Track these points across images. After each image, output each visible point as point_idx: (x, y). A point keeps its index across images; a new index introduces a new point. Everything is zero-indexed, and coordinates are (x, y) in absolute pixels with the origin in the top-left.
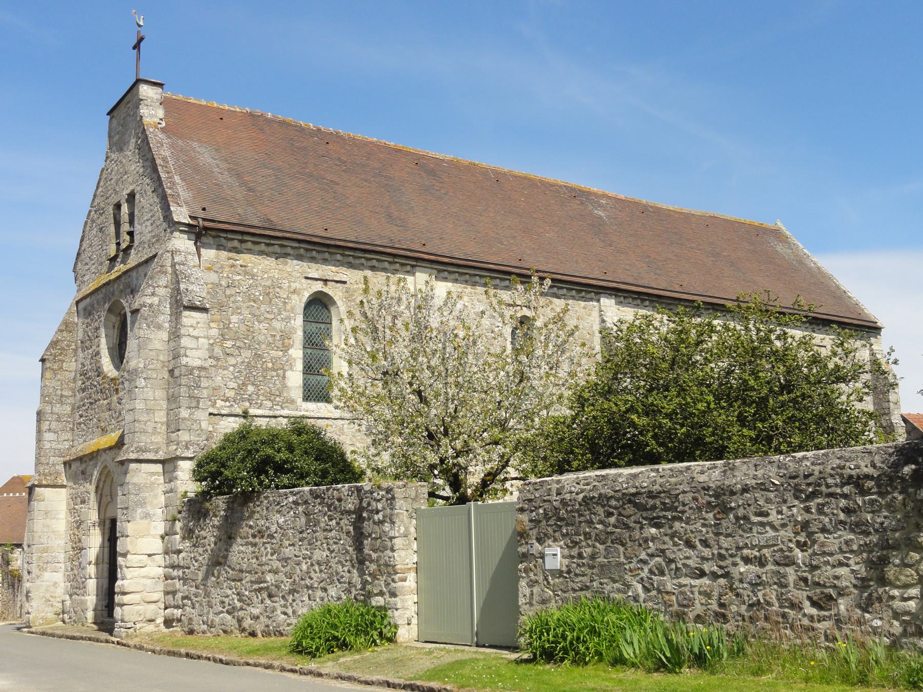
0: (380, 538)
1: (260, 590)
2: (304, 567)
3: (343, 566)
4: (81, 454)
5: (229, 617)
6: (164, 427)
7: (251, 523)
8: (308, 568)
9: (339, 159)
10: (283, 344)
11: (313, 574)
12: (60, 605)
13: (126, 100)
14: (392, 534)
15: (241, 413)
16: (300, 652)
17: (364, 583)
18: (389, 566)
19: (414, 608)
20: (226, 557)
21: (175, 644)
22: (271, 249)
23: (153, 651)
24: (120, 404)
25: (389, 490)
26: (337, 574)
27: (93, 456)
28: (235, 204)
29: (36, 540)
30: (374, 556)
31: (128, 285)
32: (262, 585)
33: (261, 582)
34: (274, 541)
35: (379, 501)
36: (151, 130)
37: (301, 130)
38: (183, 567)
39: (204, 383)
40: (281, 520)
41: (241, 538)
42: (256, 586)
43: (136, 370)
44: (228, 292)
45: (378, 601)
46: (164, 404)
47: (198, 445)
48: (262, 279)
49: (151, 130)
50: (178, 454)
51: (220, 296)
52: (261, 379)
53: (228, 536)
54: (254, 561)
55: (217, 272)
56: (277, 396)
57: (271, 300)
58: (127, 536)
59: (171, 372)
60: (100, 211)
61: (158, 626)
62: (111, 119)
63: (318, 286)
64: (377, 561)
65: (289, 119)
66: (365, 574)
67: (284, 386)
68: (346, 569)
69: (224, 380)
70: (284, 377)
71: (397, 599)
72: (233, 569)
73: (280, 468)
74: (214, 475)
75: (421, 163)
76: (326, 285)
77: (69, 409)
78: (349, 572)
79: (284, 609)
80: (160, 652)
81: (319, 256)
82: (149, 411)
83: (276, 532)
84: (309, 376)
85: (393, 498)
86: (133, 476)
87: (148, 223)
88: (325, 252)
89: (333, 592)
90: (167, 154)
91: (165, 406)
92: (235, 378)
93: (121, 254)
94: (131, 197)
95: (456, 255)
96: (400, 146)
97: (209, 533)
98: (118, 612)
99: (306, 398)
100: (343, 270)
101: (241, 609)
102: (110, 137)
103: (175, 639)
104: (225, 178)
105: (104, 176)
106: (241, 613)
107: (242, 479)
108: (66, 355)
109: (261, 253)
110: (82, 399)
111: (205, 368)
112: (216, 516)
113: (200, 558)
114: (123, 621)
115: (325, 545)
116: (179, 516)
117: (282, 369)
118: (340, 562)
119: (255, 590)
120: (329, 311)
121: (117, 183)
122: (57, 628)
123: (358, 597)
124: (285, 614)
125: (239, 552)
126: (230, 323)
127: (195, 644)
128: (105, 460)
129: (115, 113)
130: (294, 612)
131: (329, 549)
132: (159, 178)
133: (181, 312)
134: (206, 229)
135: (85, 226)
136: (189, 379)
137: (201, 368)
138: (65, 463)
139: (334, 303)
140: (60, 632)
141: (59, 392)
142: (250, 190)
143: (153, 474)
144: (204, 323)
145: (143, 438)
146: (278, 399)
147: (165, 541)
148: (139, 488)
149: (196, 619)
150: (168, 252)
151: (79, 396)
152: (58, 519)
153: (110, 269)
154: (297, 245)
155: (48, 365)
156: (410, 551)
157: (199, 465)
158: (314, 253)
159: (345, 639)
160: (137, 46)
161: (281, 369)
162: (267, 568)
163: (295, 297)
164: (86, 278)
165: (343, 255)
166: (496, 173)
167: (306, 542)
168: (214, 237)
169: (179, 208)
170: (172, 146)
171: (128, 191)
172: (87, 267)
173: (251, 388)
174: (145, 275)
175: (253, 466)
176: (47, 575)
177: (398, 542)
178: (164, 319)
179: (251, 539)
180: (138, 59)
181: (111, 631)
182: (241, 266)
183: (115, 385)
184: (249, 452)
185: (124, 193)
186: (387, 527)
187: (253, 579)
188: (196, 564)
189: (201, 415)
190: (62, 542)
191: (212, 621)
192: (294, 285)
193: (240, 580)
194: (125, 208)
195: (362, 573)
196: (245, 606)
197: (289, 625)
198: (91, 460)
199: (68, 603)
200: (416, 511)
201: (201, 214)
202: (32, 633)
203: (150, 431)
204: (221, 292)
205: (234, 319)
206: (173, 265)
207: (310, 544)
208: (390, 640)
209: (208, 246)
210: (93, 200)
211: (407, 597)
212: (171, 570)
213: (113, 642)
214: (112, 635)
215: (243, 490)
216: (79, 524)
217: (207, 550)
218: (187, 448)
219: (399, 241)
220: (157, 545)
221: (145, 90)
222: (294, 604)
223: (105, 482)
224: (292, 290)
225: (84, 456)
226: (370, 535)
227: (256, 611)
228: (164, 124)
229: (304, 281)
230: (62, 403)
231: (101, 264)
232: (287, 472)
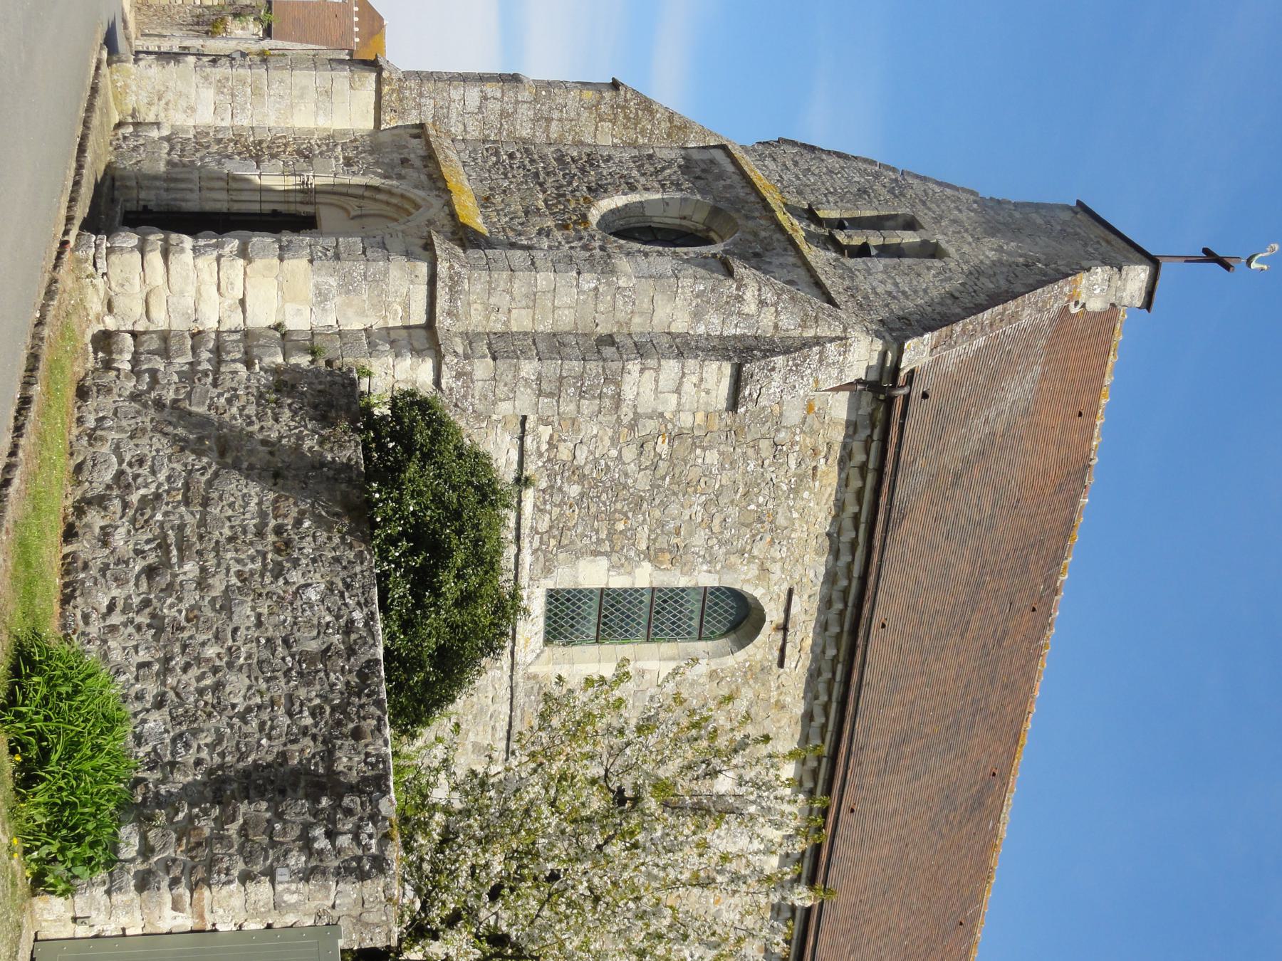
0: (273, 844)
1: (163, 546)
2: (211, 652)
3: (212, 747)
4: (441, 158)
5: (108, 477)
6: (499, 328)
7: (307, 524)
8: (208, 660)
9: (1005, 633)
10: (662, 550)
11: (194, 671)
12: (151, 118)
13: (1112, 237)
14: (282, 874)
15: (526, 473)
16: (15, 670)
17: (168, 802)
18: (209, 871)
19: (112, 929)
20: (236, 466)
21: (55, 365)
22: (848, 523)
23: (40, 323)
24: (540, 233)
25: (380, 864)
26: (195, 733)
27: (438, 183)
28: (932, 453)
29: (276, 74)
30: (232, 829)
31: (768, 247)
32: (175, 552)
33: (180, 550)
34: (268, 580)
35: (356, 838)
36: (1067, 289)
37: (1057, 559)
38: (217, 372)
39: (588, 406)
40: (312, 595)
41: (276, 501)
42: (172, 537)
43: (612, 272)
44: (765, 444)
45: (130, 841)
46: (545, 326)
47: (465, 397)
48: (790, 509)
49: (1067, 289)
50: (448, 359)
51: (755, 431)
52: (593, 510)
53: (281, 470)
54: (227, 532)
55: (804, 422)
56: (559, 540)
57: (748, 526)
58: (281, 259)
59: (609, 340)
60: (897, 189)
61: (99, 319)
62: (1068, 208)
63: (774, 614)
64: (221, 838)
65: (1077, 536)
66: (191, 806)
67: (579, 555)
68: (204, 754)
69: (593, 438)
70: (596, 553)
71: (132, 894)
72: (210, 483)
73: (423, 581)
74: (405, 438)
75: (997, 777)
76: (777, 629)
77: (525, 133)
78: (198, 762)
79: (120, 604)
80: (37, 338)
81: (832, 615)
82: (533, 299)
83: (287, 583)
84: (597, 599)
85: (363, 876)
86: (402, 268)
87: (890, 287)
88: (842, 627)
89: (155, 722)
90: (1025, 320)
91: (541, 328)
92: (596, 462)
93: (825, 232)
94: (932, 251)
95: (834, 872)
96: (1024, 740)
97: (283, 426)
98: (128, 239)
99: (552, 595)
100: (806, 660)
101: (126, 505)
102: (1037, 207)
103: (68, 363)
104: (978, 428)
105: (964, 196)
106: (116, 505)
107: (399, 501)
108: (626, 127)
109: (840, 505)
110: (543, 158)
111: (618, 407)
112: (321, 443)
113: (234, 410)
114: (110, 251)
115: (258, 700)
116: (322, 363)
117: (612, 548)
118: (220, 738)
119: (165, 537)
120: (723, 635)
121: (954, 221)
122: (107, 114)
123: (140, 789)
124: (111, 608)
125: (244, 498)
126: (704, 449)
127: (56, 396)
128: (431, 206)
129: (1081, 216)
130: (113, 629)
131: (249, 710)
132: (981, 308)
133: (730, 359)
134: (890, 401)
135: (865, 161)
136: (598, 375)
137: (618, 399)
138: (422, 126)
139: (741, 645)
140: (96, 120)
141: (556, 115)
142: (957, 477)
143: (407, 307)
144: (707, 404)
145: (478, 287)
146: (553, 542)
147: (272, 332)
148: (377, 282)
149: (108, 403)
150: (845, 330)
151: (549, 151)
152: (316, 114)
153: (791, 210)
154: (856, 574)
155: (608, 95)
156: (243, 915)
157: (424, 405)
158: (838, 606)
159: (43, 779)
160: (1209, 256)
161: (613, 547)
162: (211, 562)
163: (754, 570)
164: (768, 162)
165: (835, 660)
166: (974, 919)
167: (266, 654)
168: (872, 416)
169: (928, 349)
170: (1037, 329)
171: (943, 245)
172: (790, 164)
174: (791, 282)
175: (426, 525)
176: (209, 94)
177: (262, 891)
178: (714, 325)
179: (272, 523)
180: (1189, 260)
181: (93, 225)
182: (815, 468)
183: (573, 223)
184: (457, 515)
185: (939, 237)
186: (297, 860)
187: (188, 531)
188: (222, 400)
189: (524, 402)
190: (271, 122)
191: (102, 439)
192: (776, 568)
193: (187, 502)
194: (909, 238)
195: (191, 794)
196: (130, 513)
197: (86, 618)
198: (430, 176)
199: (155, 134)
200: (333, 925)
201: (917, 390)
202: (98, 68)
203: (492, 300)
204: (764, 430)
205: (712, 457)
206: (818, 341)
207: (260, 663)
208: (38, 883)
209: (854, 406)
210: (917, 177)
211: (138, 914)
212: (211, 345)
213: (66, 232)
214: (82, 228)
215: (376, 504)
216: (306, 155)
217: (251, 423)
218: (459, 375)
219: (860, 764)
220: (262, 316)
221: (1139, 275)
222: (131, 629)
223: (388, 203)
224: (768, 565)
225: (437, 163)
226: (279, 816)
227: (119, 539)
228: (1074, 310)
229: (785, 587)
230: (535, 120)
231: (800, 193)
232: (418, 598)
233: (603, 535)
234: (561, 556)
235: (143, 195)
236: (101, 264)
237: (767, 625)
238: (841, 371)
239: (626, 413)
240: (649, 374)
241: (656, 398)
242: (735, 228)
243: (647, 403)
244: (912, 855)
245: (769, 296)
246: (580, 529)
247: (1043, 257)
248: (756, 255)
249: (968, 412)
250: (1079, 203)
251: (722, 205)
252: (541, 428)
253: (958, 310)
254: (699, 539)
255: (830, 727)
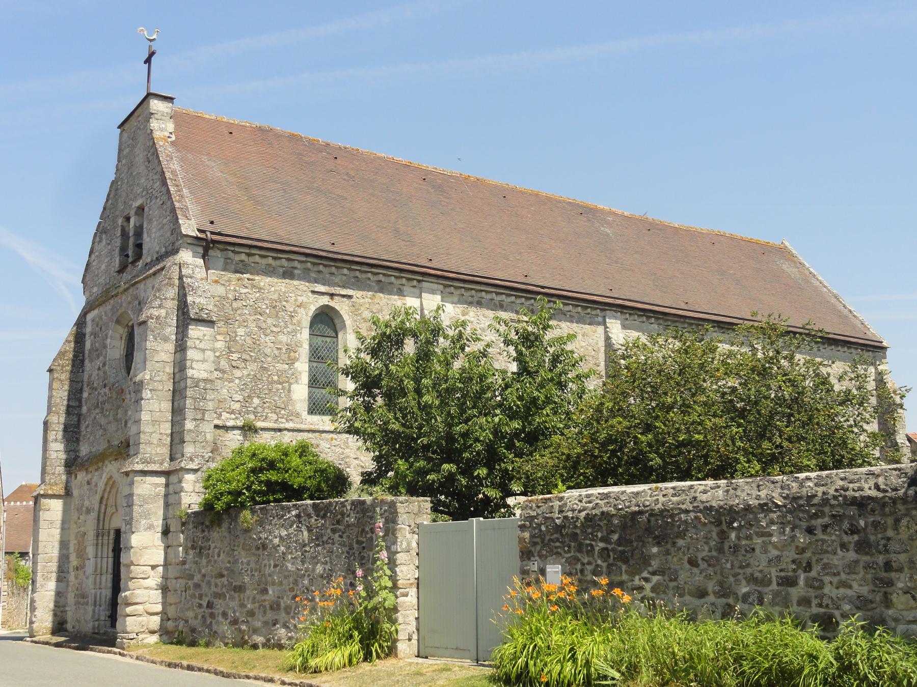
9: (347, 174)
10: (289, 357)
44: (235, 305)
49: (161, 143)
50: (183, 465)
56: (283, 408)
62: (121, 132)
63: (325, 300)
67: (290, 399)
69: (230, 392)
70: (289, 391)
75: (426, 177)
84: (314, 390)
86: (137, 487)
92: (242, 390)
95: (463, 270)
99: (311, 411)
102: (120, 150)
111: (211, 381)
126: (236, 336)
129: (126, 126)
132: (168, 191)
137: (206, 381)
145: (149, 449)
146: (283, 412)
154: (304, 259)
155: (56, 375)
158: (321, 268)
160: (148, 61)
161: (286, 381)
163: (301, 311)
165: (350, 269)
168: (222, 250)
170: (182, 160)
173: (256, 401)
178: (171, 331)
192: (300, 299)
204: (228, 305)
205: (241, 331)
206: (181, 278)
218: (192, 460)
223: (110, 492)
224: (298, 303)
228: (173, 138)
233: (280, 387)
234: (290, 408)
235: (103, 618)
236: (133, 635)
237: (330, 304)
238: (197, 266)
239: (216, 374)
240: (194, 365)
241: (207, 361)
242: (126, 313)
243: (209, 366)
244: (462, 226)
245: (158, 302)
246: (276, 398)
247: (146, 153)
248: (139, 304)
249: (223, 198)
250: (119, 127)
251: (115, 319)
252: (223, 417)
253: (169, 203)
254: (284, 338)
255: (385, 272)
